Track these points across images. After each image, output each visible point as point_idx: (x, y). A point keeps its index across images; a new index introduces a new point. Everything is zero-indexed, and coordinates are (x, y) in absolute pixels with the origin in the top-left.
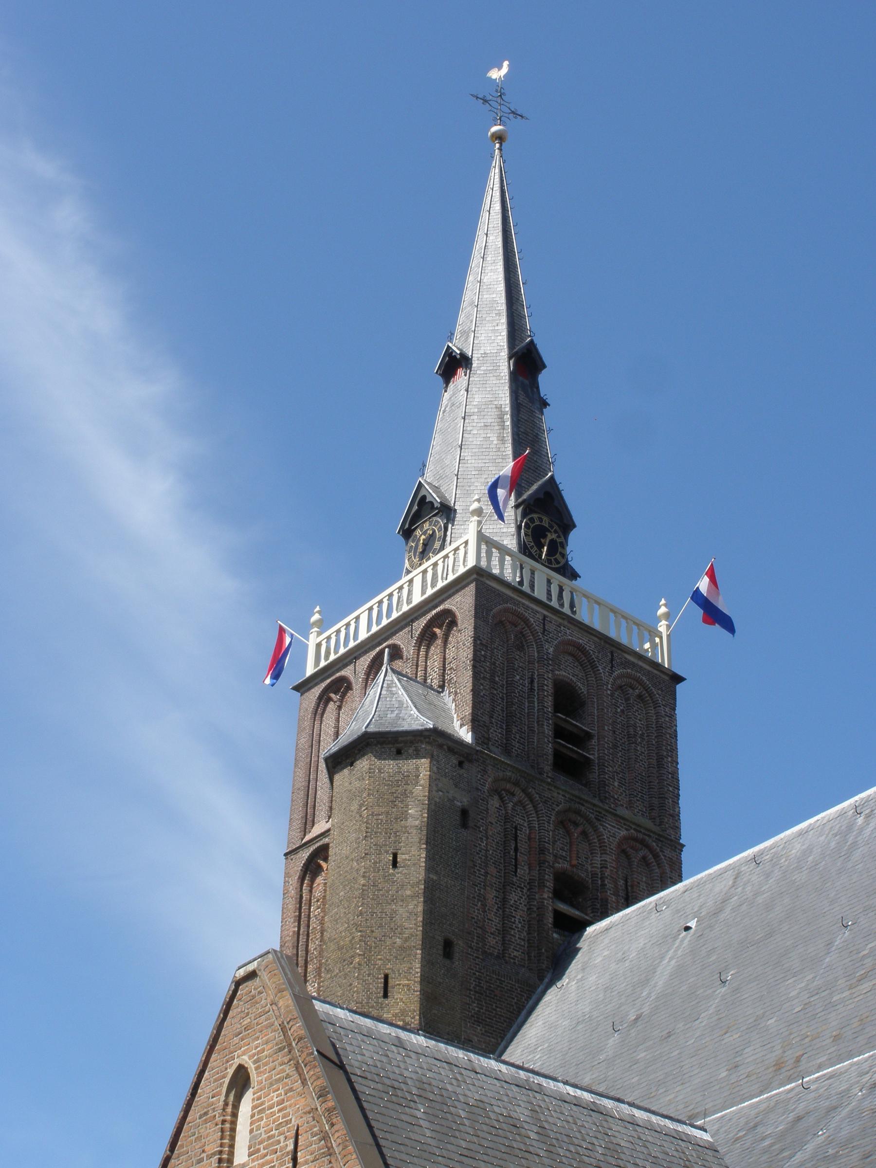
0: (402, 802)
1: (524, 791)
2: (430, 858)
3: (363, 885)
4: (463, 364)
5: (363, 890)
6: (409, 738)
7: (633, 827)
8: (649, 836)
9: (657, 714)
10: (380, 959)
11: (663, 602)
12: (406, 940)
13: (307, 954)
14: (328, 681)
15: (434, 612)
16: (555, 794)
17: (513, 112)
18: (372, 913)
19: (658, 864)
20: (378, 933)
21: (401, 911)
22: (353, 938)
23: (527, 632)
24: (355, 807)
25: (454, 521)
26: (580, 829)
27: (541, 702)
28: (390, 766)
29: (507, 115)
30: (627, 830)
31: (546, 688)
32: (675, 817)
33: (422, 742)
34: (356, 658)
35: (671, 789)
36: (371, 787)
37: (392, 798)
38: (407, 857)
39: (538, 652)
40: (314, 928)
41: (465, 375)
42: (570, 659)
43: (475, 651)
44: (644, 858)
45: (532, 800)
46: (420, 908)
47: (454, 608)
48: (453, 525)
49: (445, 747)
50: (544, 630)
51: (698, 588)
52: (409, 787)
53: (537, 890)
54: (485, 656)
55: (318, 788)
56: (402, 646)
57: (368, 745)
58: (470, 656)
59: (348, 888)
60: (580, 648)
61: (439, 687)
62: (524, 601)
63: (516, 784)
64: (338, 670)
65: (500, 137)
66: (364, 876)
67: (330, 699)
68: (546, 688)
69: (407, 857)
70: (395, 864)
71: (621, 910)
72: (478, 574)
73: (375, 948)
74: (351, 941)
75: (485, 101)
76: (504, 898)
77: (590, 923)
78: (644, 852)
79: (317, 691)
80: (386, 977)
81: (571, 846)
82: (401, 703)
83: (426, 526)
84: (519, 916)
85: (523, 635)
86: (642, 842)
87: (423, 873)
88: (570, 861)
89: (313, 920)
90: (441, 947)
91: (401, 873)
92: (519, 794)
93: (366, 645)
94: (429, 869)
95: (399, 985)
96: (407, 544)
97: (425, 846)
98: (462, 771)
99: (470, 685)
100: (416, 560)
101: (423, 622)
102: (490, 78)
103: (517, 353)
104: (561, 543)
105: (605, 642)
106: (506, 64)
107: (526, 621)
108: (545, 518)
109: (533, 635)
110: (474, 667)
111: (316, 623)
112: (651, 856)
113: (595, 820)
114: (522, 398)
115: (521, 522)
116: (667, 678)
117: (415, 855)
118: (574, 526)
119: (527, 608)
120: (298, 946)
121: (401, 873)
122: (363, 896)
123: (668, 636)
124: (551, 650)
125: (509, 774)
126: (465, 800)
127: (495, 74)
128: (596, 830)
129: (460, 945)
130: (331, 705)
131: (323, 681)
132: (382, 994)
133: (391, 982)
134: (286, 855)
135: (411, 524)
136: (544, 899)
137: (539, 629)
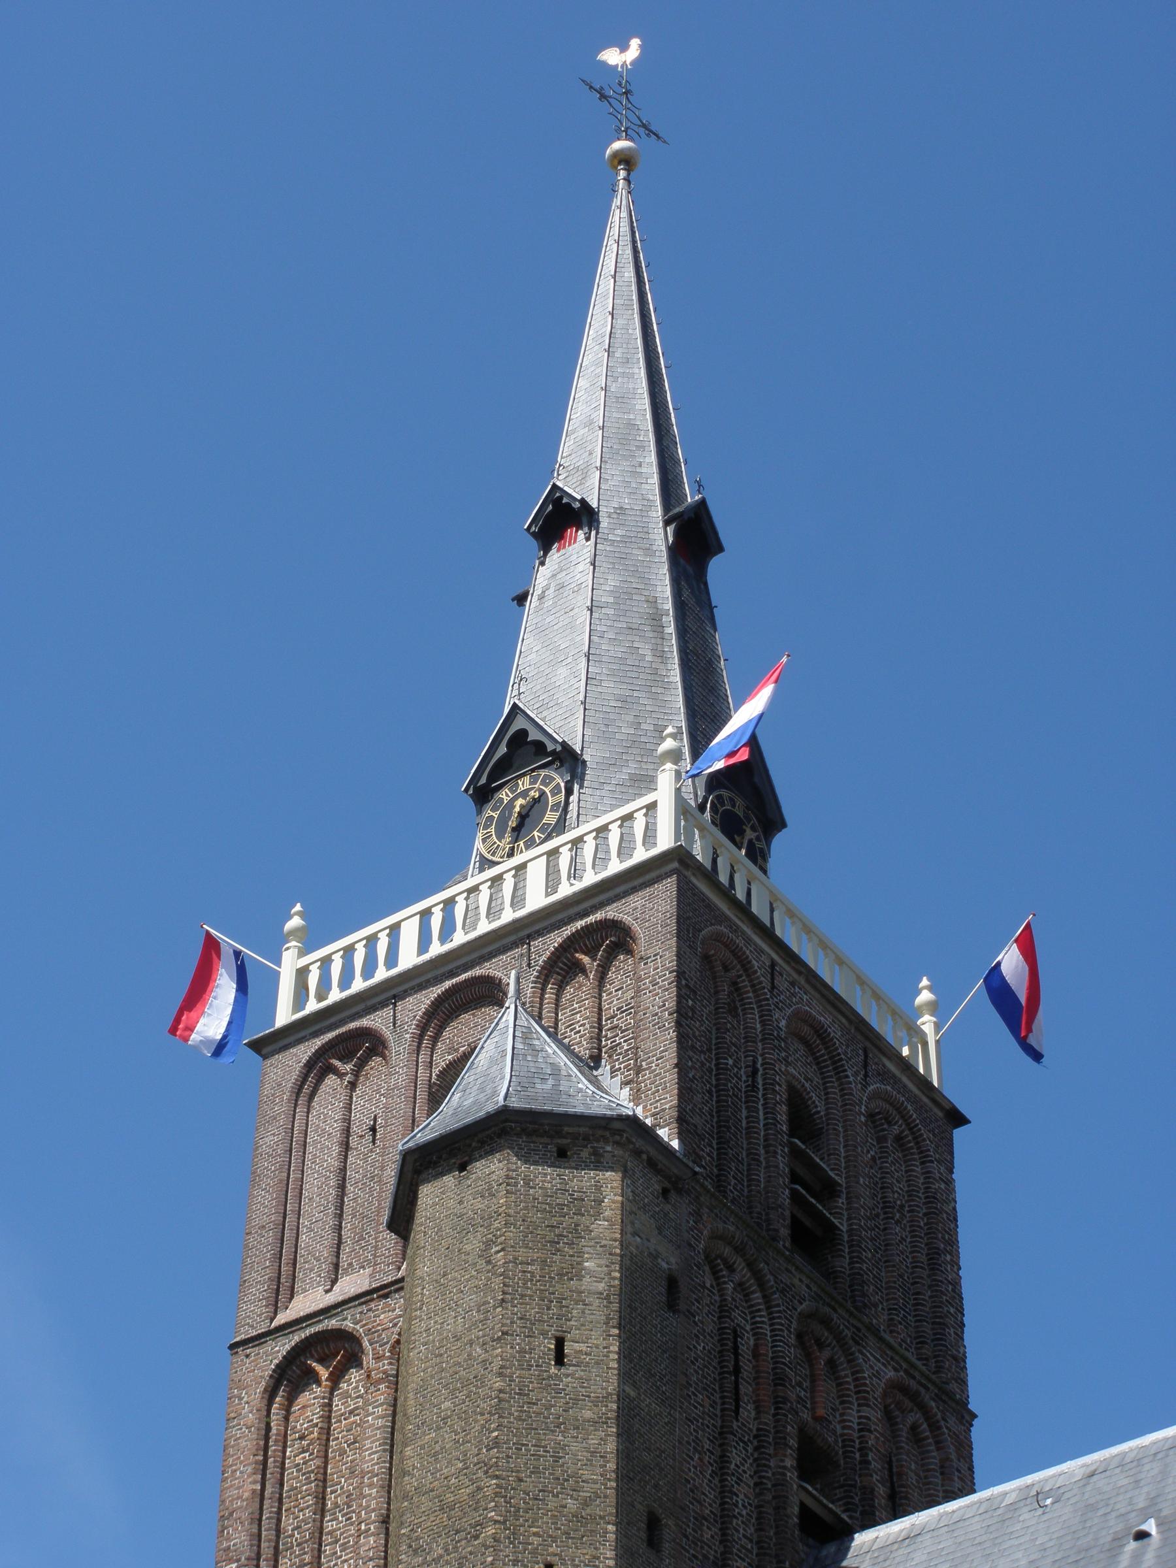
0: (571, 1244)
1: (750, 1265)
2: (626, 1355)
3: (501, 1391)
4: (584, 520)
6: (582, 1130)
7: (905, 1366)
8: (927, 1389)
9: (927, 1174)
10: (536, 1534)
11: (925, 982)
12: (586, 1503)
13: (278, 1536)
14: (330, 1035)
15: (580, 924)
16: (796, 1281)
17: (644, 126)
18: (519, 1446)
19: (937, 1443)
20: (529, 1483)
21: (575, 1447)
22: (479, 1489)
23: (745, 983)
24: (473, 1244)
25: (582, 780)
26: (827, 1353)
27: (770, 1111)
28: (546, 1176)
29: (636, 128)
30: (896, 1370)
31: (777, 1088)
32: (960, 1361)
33: (606, 1141)
34: (398, 997)
35: (952, 1310)
36: (511, 1212)
38: (583, 1347)
39: (763, 1023)
40: (293, 1489)
41: (588, 539)
42: (801, 1047)
43: (680, 997)
44: (914, 1428)
45: (762, 1285)
46: (611, 1446)
47: (627, 919)
48: (581, 787)
49: (644, 1157)
50: (773, 987)
51: (999, 964)
54: (693, 1009)
55: (303, 1230)
57: (503, 1133)
58: (671, 1004)
60: (821, 1033)
61: (591, 1057)
62: (745, 928)
63: (739, 1250)
64: (353, 1018)
65: (625, 160)
66: (500, 1374)
67: (329, 1069)
68: (777, 1088)
69: (583, 1347)
70: (560, 1358)
71: (939, 1504)
72: (681, 862)
74: (472, 1495)
75: (603, 97)
76: (722, 1456)
77: (869, 1521)
78: (915, 1417)
79: (305, 1051)
81: (813, 1381)
82: (556, 1071)
83: (524, 784)
84: (743, 1494)
85: (737, 990)
86: (914, 1397)
87: (614, 1380)
88: (813, 1409)
89: (291, 1472)
90: (643, 1526)
91: (572, 1375)
92: (742, 1272)
94: (625, 1375)
96: (479, 812)
97: (616, 1331)
98: (668, 1207)
99: (671, 1056)
100: (505, 843)
101: (555, 939)
102: (604, 64)
103: (679, 516)
104: (762, 851)
105: (857, 1029)
106: (635, 43)
107: (746, 965)
108: (739, 802)
109: (754, 992)
110: (678, 1024)
111: (294, 932)
112: (925, 1426)
113: (851, 1342)
114: (686, 593)
115: (705, 799)
116: (940, 1114)
117: (597, 1345)
118: (784, 825)
119: (748, 941)
120: (260, 1520)
121: (572, 1375)
123: (937, 1042)
124: (783, 1023)
125: (732, 1228)
126: (673, 1260)
127: (612, 57)
128: (851, 1361)
129: (669, 1526)
130: (331, 1081)
131: (316, 1034)
135: (492, 777)
136: (785, 1468)
137: (766, 982)
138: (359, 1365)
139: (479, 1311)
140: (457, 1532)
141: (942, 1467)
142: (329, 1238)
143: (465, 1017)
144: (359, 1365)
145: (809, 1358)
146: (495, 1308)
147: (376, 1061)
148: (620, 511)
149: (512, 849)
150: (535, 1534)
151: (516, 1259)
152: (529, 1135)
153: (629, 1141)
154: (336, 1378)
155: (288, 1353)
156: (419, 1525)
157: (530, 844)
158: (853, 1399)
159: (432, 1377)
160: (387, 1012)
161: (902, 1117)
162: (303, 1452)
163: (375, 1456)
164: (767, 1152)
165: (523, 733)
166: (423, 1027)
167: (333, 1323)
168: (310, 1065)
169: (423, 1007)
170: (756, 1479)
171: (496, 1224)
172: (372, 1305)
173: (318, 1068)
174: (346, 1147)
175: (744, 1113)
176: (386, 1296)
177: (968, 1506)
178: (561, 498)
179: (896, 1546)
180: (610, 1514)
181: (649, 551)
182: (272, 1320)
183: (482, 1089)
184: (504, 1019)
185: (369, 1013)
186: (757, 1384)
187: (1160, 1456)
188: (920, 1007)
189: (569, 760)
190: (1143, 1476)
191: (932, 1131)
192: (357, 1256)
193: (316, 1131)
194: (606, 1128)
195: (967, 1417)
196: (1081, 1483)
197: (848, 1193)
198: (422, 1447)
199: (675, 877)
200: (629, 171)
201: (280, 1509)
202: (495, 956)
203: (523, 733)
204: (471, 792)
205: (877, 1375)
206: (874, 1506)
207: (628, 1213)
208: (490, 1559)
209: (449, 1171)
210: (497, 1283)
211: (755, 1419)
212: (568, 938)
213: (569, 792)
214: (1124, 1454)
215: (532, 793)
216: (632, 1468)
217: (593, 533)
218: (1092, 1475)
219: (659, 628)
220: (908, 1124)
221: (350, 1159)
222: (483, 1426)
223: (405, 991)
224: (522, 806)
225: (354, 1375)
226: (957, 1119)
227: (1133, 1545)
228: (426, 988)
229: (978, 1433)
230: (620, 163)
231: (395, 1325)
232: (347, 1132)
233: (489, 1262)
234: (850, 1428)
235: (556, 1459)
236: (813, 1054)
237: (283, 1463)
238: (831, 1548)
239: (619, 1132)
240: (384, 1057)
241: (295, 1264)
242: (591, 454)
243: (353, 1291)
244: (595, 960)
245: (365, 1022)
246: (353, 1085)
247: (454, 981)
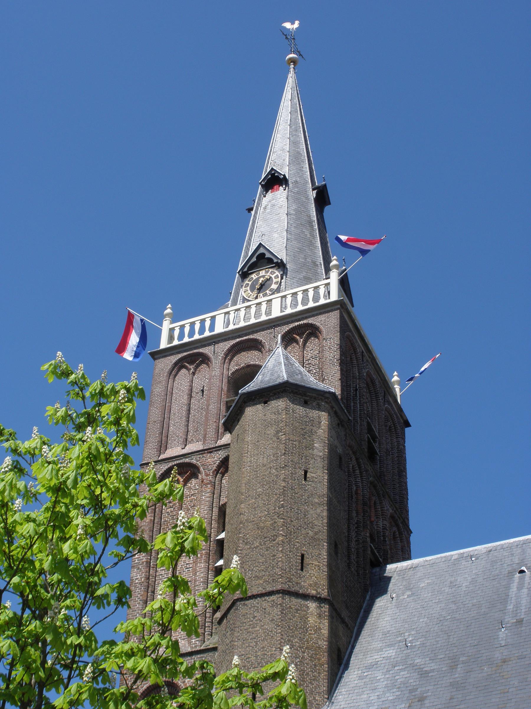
1: (357, 459)
3: (284, 487)
4: (284, 182)
5: (284, 490)
6: (314, 395)
11: (395, 373)
12: (316, 533)
14: (185, 354)
15: (297, 324)
17: (298, 51)
18: (291, 508)
20: (295, 523)
21: (311, 512)
22: (275, 522)
24: (271, 431)
28: (300, 410)
33: (322, 400)
36: (288, 421)
40: (165, 521)
41: (285, 190)
45: (360, 468)
46: (325, 514)
47: (318, 324)
52: (315, 428)
53: (362, 529)
56: (263, 341)
57: (285, 391)
58: (338, 356)
59: (267, 487)
60: (373, 381)
63: (354, 453)
66: (284, 481)
72: (341, 305)
73: (294, 533)
74: (272, 525)
75: (286, 38)
80: (303, 556)
83: (263, 273)
87: (326, 489)
93: (228, 335)
95: (312, 564)
96: (243, 281)
99: (338, 375)
101: (286, 328)
102: (285, 28)
111: (168, 315)
112: (397, 533)
116: (402, 421)
117: (320, 476)
119: (357, 341)
120: (153, 531)
122: (284, 493)
127: (287, 25)
130: (184, 371)
132: (300, 568)
133: (306, 561)
138: (197, 477)
139: (274, 456)
140: (265, 538)
141: (402, 549)
142: (183, 429)
143: (243, 353)
144: (197, 477)
146: (281, 456)
147: (204, 366)
148: (296, 182)
149: (257, 296)
150: (297, 542)
151: (289, 438)
152: (294, 393)
153: (330, 402)
155: (167, 469)
156: (248, 534)
157: (265, 295)
158: (381, 517)
159: (253, 479)
160: (211, 348)
161: (392, 419)
162: (171, 508)
163: (206, 512)
164: (361, 420)
165: (263, 255)
166: (226, 355)
167: (187, 460)
168: (176, 364)
169: (227, 348)
170: (356, 539)
171: (281, 425)
172: (205, 455)
173: (179, 365)
174: (190, 396)
175: (352, 404)
176: (211, 452)
177: (436, 559)
178: (274, 173)
179: (407, 570)
180: (325, 539)
181: (307, 198)
182: (159, 456)
183: (272, 375)
184: (277, 351)
185: (203, 347)
186: (357, 504)
187: (519, 546)
188: (394, 382)
189: (281, 265)
190: (515, 552)
191: (400, 426)
192: (195, 437)
193: (177, 389)
194: (322, 396)
195: (410, 532)
196: (486, 554)
197: (379, 442)
198: (249, 505)
199: (338, 311)
200: (295, 65)
201: (160, 528)
202: (259, 332)
203: (263, 255)
204: (241, 273)
205: (388, 510)
206: (387, 557)
207: (331, 427)
208: (280, 549)
209: (260, 403)
210: (282, 446)
211: (356, 517)
212: (292, 328)
213: (282, 278)
214: (502, 545)
215: (267, 277)
216: (332, 524)
217: (287, 188)
218: (490, 551)
219: (312, 226)
220: (393, 422)
221: (192, 401)
222: (276, 499)
223: (219, 341)
224: (262, 281)
225: (193, 481)
226: (407, 424)
227: (518, 575)
228: (228, 340)
229: (412, 538)
230: (291, 62)
231: (215, 464)
232: (191, 391)
233: (278, 439)
234: (380, 527)
235: (305, 515)
236: (369, 389)
237: (162, 511)
238: (378, 569)
239: (328, 398)
240: (208, 364)
241: (167, 437)
242: (284, 160)
243: (195, 449)
244: (302, 338)
245: (201, 350)
246: (194, 374)
247: (241, 339)
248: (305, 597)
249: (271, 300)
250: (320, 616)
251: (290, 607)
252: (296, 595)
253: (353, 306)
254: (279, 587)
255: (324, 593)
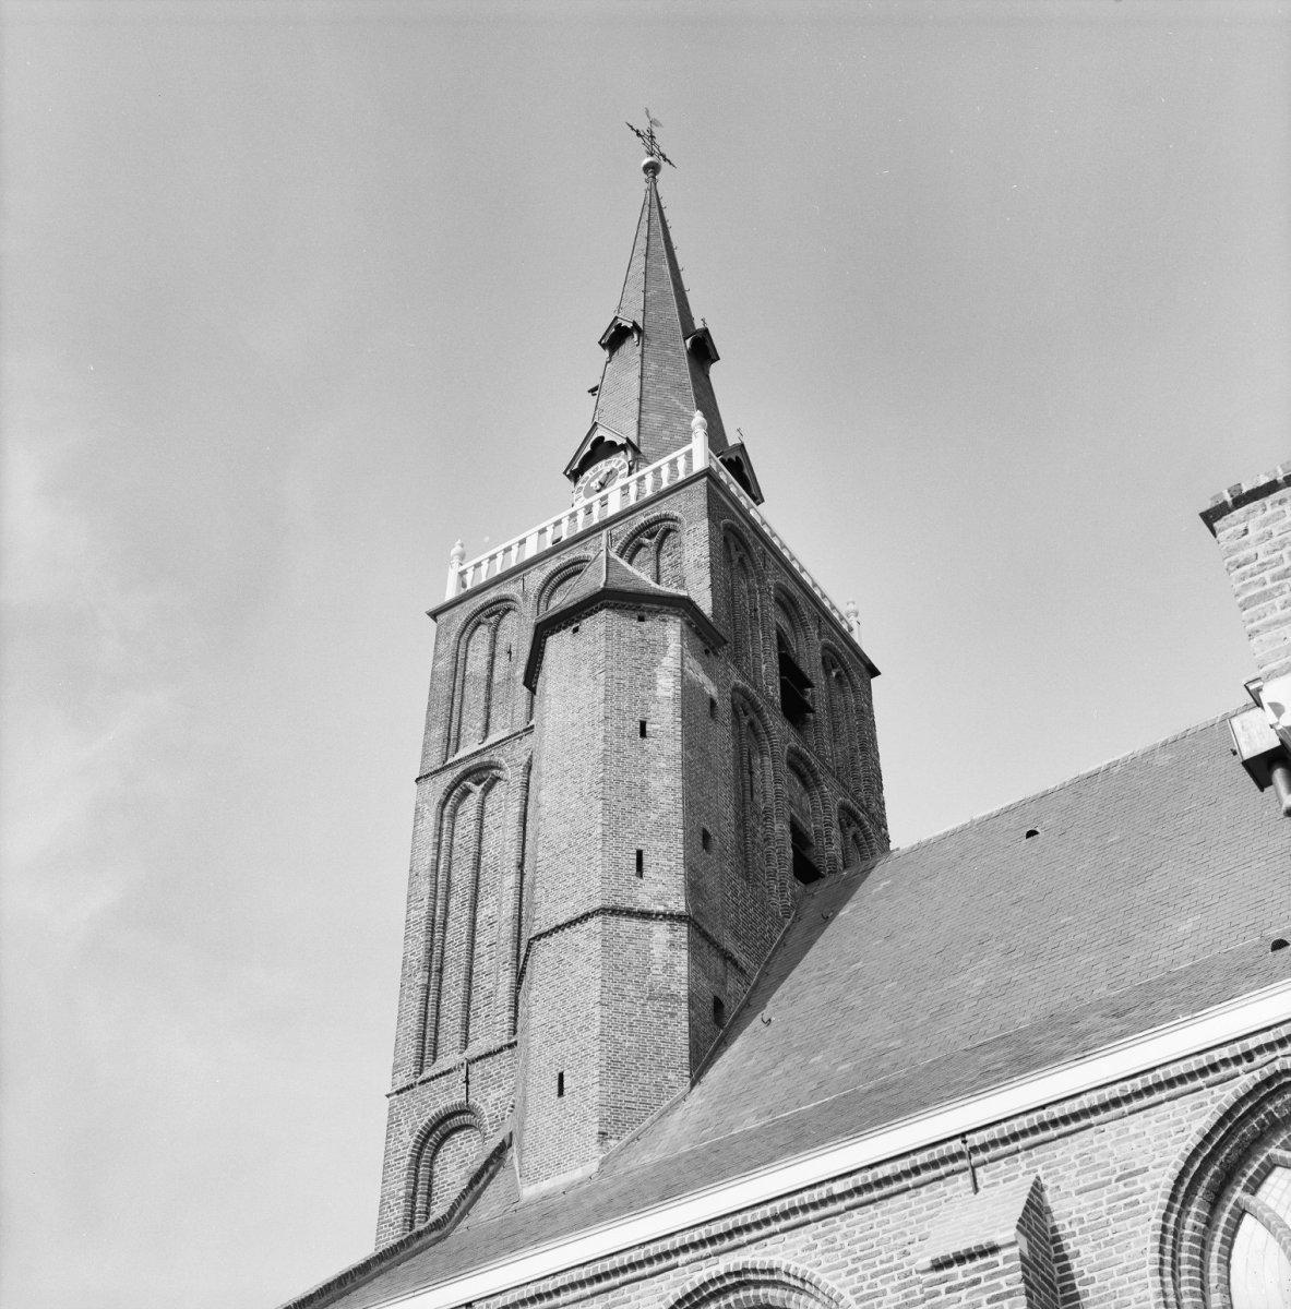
0: (649, 670)
24: (585, 671)
37: (635, 664)
46: (679, 783)
80: (639, 854)
97: (680, 719)
122: (604, 759)
133: (646, 861)
134: (417, 780)
145: (827, 672)
154: (487, 791)
167: (486, 758)
199: (705, 479)
226: (874, 672)
248: (646, 915)
249: (605, 497)
250: (672, 945)
251: (618, 935)
252: (630, 913)
253: (757, 498)
254: (597, 904)
255: (679, 905)
